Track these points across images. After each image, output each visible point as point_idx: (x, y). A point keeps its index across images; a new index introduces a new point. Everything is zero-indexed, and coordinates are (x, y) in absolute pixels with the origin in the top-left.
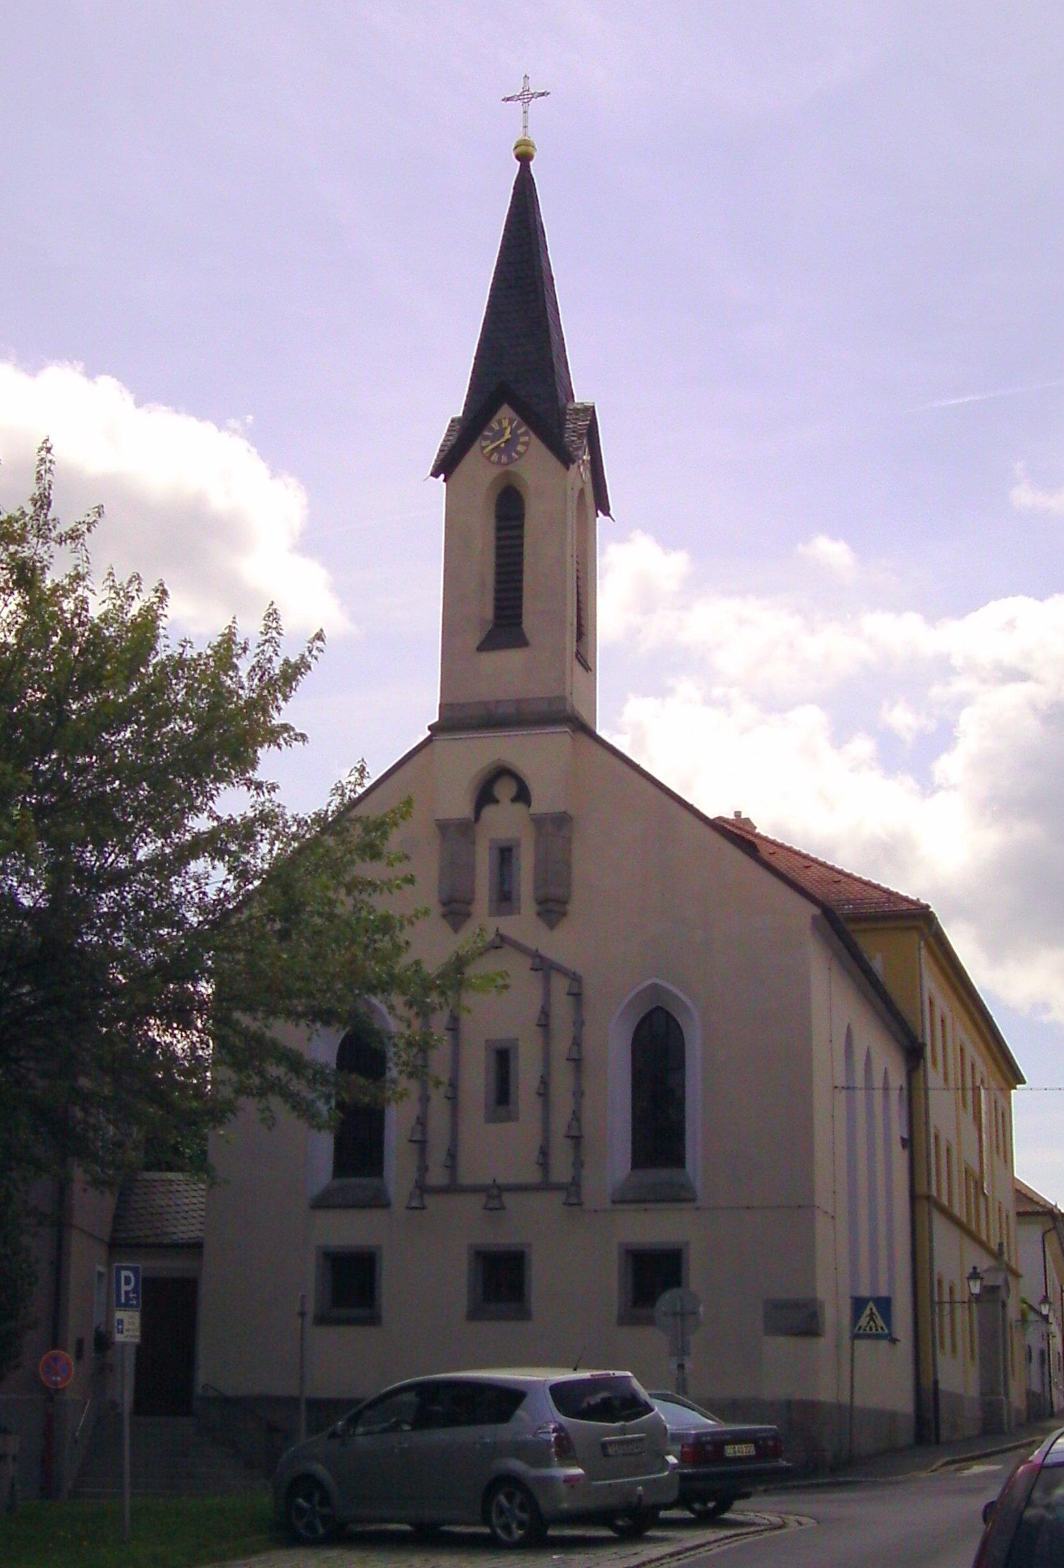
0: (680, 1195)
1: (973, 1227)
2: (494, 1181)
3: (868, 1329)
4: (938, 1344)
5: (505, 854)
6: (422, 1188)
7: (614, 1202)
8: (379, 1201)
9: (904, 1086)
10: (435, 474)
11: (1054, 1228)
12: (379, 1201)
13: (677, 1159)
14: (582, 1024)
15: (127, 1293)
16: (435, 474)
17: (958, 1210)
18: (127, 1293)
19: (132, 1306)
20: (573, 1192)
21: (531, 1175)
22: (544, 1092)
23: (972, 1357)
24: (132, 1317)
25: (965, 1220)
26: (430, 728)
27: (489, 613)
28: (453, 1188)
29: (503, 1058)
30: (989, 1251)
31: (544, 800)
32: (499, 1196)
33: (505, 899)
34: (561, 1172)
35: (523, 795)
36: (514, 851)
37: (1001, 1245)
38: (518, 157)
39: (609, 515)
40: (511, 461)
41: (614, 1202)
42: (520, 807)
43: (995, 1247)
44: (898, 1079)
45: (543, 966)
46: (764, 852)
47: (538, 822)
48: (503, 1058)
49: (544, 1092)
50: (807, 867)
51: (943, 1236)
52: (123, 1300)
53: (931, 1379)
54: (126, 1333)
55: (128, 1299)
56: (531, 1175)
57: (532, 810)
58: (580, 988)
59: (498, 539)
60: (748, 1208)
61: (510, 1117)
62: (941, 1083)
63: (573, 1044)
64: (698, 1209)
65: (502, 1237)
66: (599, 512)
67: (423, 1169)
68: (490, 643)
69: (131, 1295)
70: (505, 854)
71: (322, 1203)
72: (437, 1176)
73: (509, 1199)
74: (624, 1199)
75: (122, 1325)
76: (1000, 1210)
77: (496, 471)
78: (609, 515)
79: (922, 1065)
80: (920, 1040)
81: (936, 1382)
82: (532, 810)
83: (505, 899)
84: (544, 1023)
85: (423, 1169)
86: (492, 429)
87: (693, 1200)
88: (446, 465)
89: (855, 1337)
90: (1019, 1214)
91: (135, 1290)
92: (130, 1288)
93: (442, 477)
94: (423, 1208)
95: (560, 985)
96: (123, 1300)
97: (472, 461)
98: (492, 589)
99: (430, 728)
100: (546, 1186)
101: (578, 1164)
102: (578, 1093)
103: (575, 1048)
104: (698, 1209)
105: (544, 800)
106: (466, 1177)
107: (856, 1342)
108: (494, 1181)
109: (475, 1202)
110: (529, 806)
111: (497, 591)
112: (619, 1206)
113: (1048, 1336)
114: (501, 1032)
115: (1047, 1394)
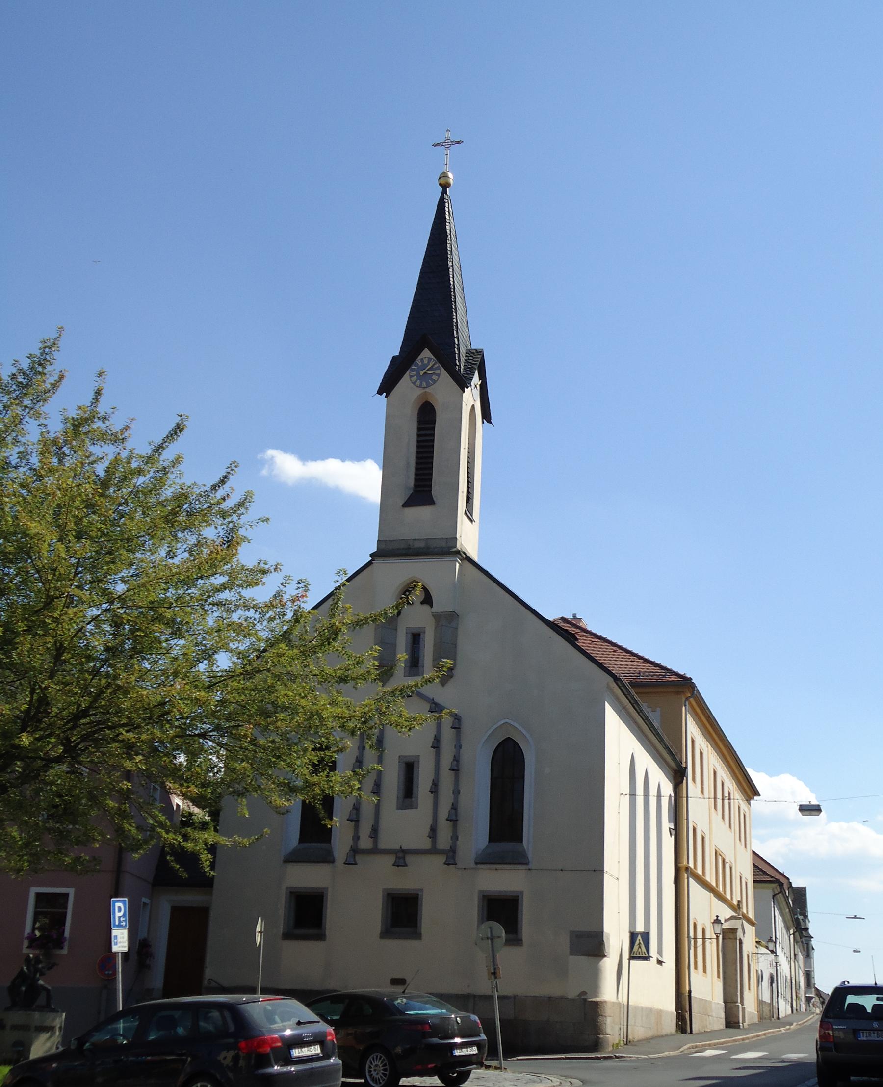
0: (519, 859)
1: (721, 889)
2: (401, 847)
3: (638, 953)
4: (760, 980)
5: (416, 638)
6: (355, 851)
7: (476, 863)
8: (327, 858)
9: (673, 795)
10: (380, 392)
11: (781, 892)
12: (327, 858)
13: (518, 837)
14: (460, 747)
15: (119, 917)
16: (380, 392)
17: (710, 878)
18: (119, 917)
19: (122, 926)
20: (451, 857)
21: (426, 844)
22: (435, 789)
23: (719, 977)
24: (122, 934)
25: (714, 884)
26: (371, 555)
27: (411, 483)
28: (375, 851)
29: (409, 768)
30: (732, 907)
31: (441, 604)
32: (404, 858)
33: (414, 665)
34: (444, 841)
35: (428, 600)
36: (422, 635)
37: (739, 901)
38: (441, 185)
39: (491, 423)
40: (428, 386)
41: (476, 863)
42: (426, 607)
43: (735, 903)
44: (668, 789)
45: (436, 708)
46: (583, 641)
47: (437, 617)
48: (409, 768)
49: (435, 789)
50: (614, 651)
51: (696, 893)
52: (117, 923)
53: (687, 989)
54: (119, 945)
55: (120, 922)
56: (426, 844)
57: (434, 610)
58: (460, 724)
59: (418, 435)
60: (562, 870)
61: (410, 807)
62: (699, 794)
63: (454, 760)
64: (529, 869)
65: (404, 882)
66: (484, 420)
67: (356, 838)
68: (409, 503)
69: (122, 919)
70: (416, 638)
71: (293, 858)
72: (365, 843)
73: (409, 859)
74: (486, 859)
75: (117, 939)
76: (741, 878)
77: (419, 392)
78: (491, 423)
79: (685, 782)
80: (684, 765)
81: (690, 992)
82: (434, 610)
83: (414, 665)
84: (436, 745)
85: (356, 838)
86: (417, 365)
87: (527, 864)
88: (387, 386)
89: (632, 958)
90: (755, 882)
91: (124, 915)
92: (121, 914)
93: (385, 394)
94: (356, 864)
95: (447, 721)
96: (117, 923)
97: (406, 385)
98: (414, 474)
99: (371, 555)
100: (434, 851)
101: (455, 838)
102: (457, 792)
103: (455, 762)
104: (529, 869)
105: (441, 604)
106: (382, 845)
107: (632, 962)
108: (401, 847)
109: (391, 859)
110: (432, 606)
111: (417, 469)
112: (479, 866)
113: (776, 964)
114: (410, 751)
115: (775, 1004)
